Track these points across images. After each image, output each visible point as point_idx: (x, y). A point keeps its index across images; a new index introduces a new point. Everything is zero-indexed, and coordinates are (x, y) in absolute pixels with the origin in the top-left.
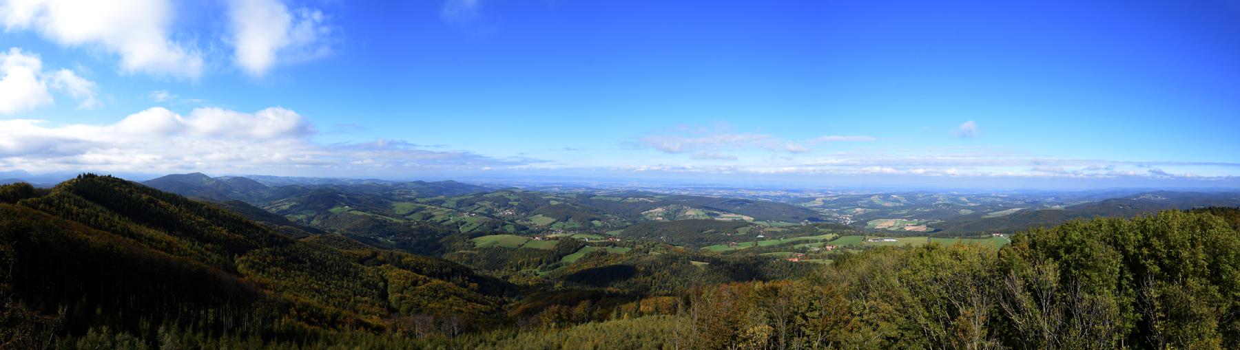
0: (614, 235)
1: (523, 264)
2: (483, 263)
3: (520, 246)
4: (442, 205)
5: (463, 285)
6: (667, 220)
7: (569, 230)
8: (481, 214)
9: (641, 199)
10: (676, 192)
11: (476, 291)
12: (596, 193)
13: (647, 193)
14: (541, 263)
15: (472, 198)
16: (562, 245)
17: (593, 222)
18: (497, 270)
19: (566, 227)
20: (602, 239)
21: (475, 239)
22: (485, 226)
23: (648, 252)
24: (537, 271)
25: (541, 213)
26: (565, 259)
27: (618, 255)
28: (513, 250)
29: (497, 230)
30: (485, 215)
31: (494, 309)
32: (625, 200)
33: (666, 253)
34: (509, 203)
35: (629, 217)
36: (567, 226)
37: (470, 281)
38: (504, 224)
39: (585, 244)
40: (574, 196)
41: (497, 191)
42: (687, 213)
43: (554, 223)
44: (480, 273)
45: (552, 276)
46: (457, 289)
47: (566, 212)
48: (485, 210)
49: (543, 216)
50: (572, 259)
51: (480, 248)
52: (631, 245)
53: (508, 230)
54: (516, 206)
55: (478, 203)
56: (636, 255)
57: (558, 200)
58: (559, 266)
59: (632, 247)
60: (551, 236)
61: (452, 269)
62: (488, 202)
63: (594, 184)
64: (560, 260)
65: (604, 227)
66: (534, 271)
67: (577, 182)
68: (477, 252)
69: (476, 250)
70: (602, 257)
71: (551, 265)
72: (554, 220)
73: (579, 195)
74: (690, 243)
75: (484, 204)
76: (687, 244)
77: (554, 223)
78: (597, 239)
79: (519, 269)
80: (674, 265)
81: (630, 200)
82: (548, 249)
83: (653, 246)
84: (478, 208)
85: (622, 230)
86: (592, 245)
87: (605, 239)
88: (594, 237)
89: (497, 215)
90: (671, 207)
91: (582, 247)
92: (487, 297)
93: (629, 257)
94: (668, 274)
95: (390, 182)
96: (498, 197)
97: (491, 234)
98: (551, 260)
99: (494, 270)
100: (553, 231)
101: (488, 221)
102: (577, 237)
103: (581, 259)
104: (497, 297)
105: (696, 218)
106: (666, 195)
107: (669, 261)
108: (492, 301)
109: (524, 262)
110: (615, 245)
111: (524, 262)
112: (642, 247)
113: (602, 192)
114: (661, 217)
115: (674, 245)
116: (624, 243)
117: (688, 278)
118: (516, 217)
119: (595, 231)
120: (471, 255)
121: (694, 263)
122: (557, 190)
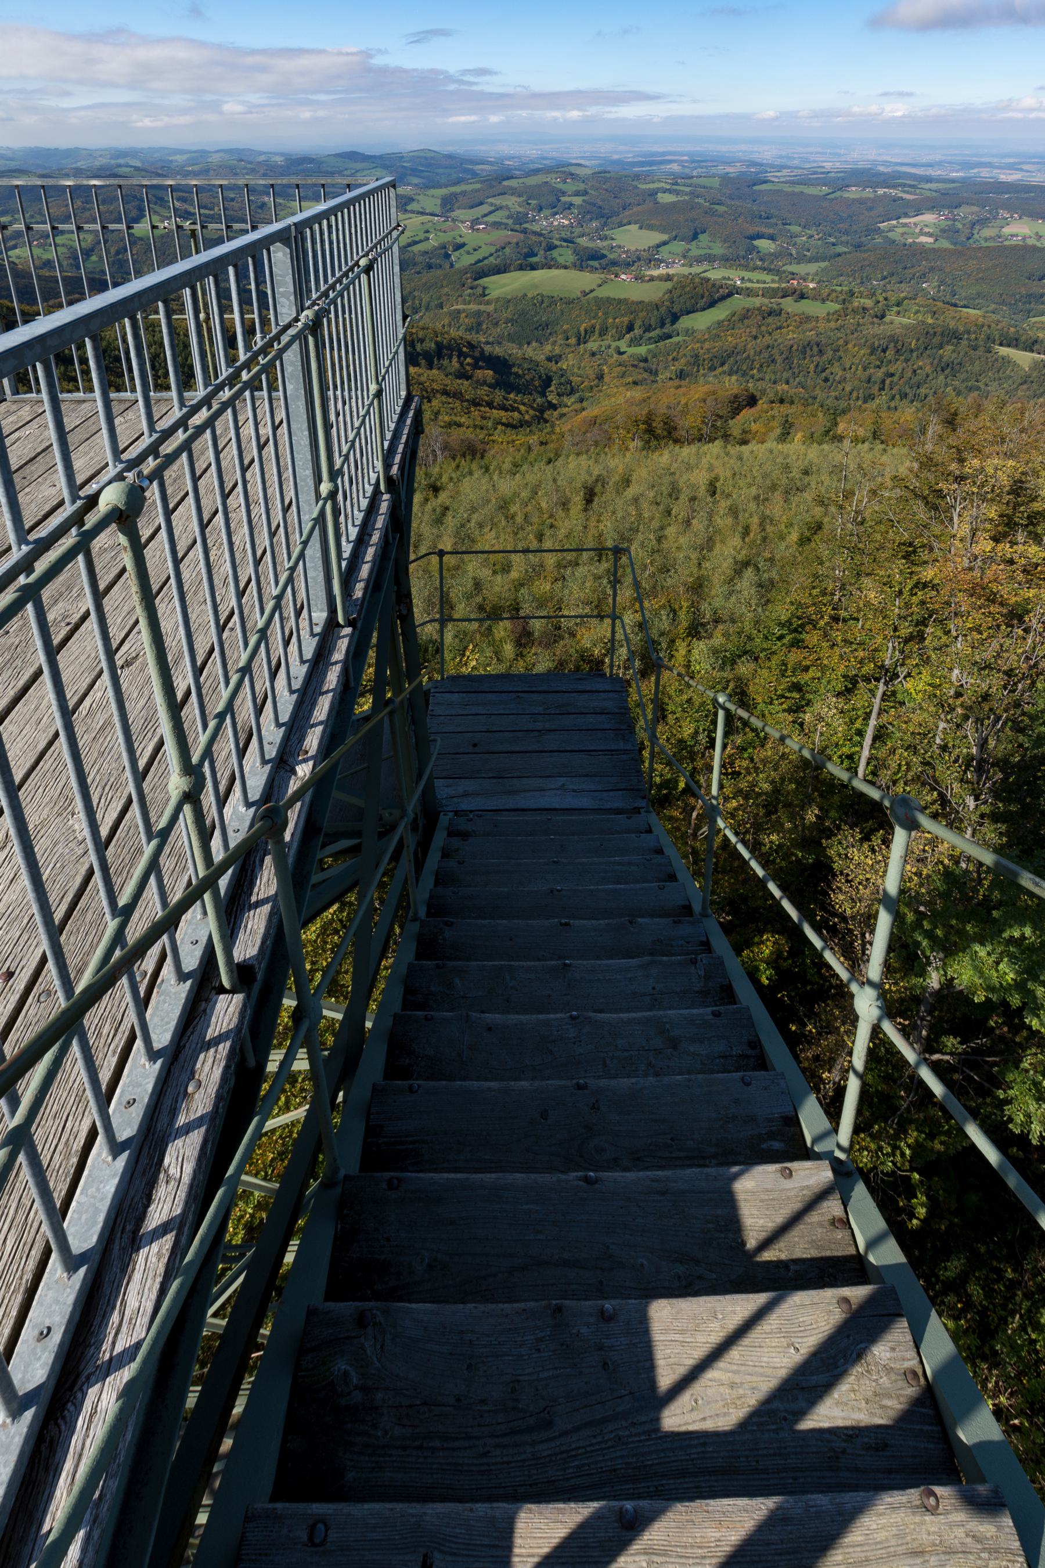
0: (803, 273)
1: (589, 332)
2: (502, 329)
3: (585, 294)
4: (409, 208)
5: (463, 375)
6: (945, 244)
7: (699, 260)
8: (497, 225)
9: (881, 192)
10: (985, 174)
11: (490, 386)
12: (769, 176)
13: (900, 175)
14: (630, 328)
15: (477, 191)
16: (678, 292)
17: (756, 243)
18: (534, 344)
19: (691, 254)
20: (773, 281)
21: (485, 281)
22: (507, 250)
23: (883, 316)
24: (623, 345)
25: (635, 223)
26: (685, 322)
27: (808, 319)
28: (570, 302)
29: (534, 260)
30: (506, 226)
31: (527, 417)
32: (838, 194)
33: (930, 321)
34: (563, 199)
35: (846, 233)
36: (695, 252)
37: (475, 366)
38: (551, 247)
39: (738, 291)
40: (716, 182)
41: (536, 172)
42: (1007, 231)
43: (665, 243)
44: (498, 351)
45: (654, 356)
46: (447, 381)
47: (693, 220)
48: (508, 217)
49: (641, 228)
50: (702, 321)
51: (498, 300)
52: (842, 297)
53: (561, 260)
54: (580, 207)
55: (490, 200)
56: (851, 320)
57: (677, 193)
58: (670, 337)
59: (844, 301)
60: (655, 273)
61: (437, 343)
62: (514, 199)
63: (767, 154)
64: (673, 322)
65: (776, 256)
66: (614, 344)
67: (724, 148)
68: (490, 308)
69: (488, 303)
70: (770, 320)
71: (653, 334)
72: (665, 237)
73: (726, 179)
74: (1003, 303)
75: (504, 204)
76: (993, 306)
77: (665, 243)
78: (769, 281)
79: (582, 340)
80: (948, 350)
81: (853, 193)
82: (647, 300)
83: (898, 304)
84: (491, 213)
85: (823, 265)
86: (749, 293)
87: (779, 282)
88: (756, 276)
89: (536, 228)
90: (962, 212)
91: (724, 298)
92: (512, 396)
93: (833, 324)
94: (928, 369)
95: (282, 154)
96: (538, 186)
97: (521, 268)
98: (653, 323)
99: (528, 344)
100: (662, 261)
101: (515, 240)
102: (716, 274)
103: (720, 323)
104: (536, 395)
105: (1030, 242)
106: (953, 181)
107: (936, 341)
108: (524, 404)
109: (593, 327)
110: (802, 296)
111: (593, 327)
112: (868, 303)
113: (785, 172)
114: (930, 235)
115: (955, 305)
116: (825, 292)
117: (981, 385)
118: (578, 231)
119: (759, 263)
120: (479, 313)
121: (1004, 351)
122: (675, 167)
